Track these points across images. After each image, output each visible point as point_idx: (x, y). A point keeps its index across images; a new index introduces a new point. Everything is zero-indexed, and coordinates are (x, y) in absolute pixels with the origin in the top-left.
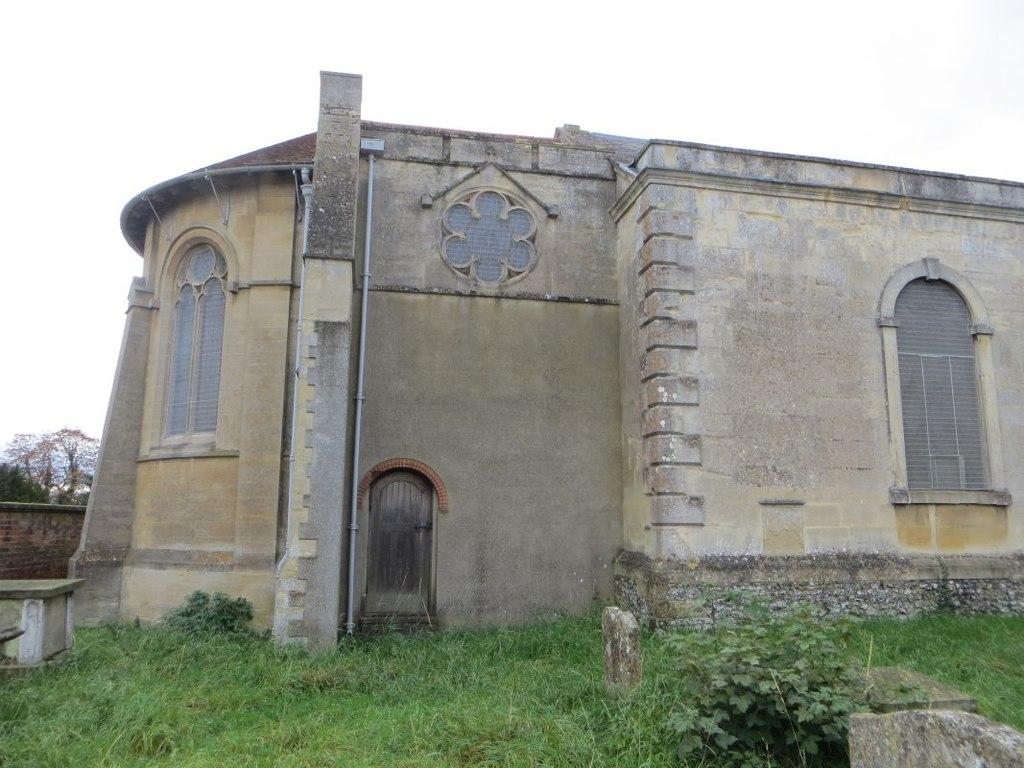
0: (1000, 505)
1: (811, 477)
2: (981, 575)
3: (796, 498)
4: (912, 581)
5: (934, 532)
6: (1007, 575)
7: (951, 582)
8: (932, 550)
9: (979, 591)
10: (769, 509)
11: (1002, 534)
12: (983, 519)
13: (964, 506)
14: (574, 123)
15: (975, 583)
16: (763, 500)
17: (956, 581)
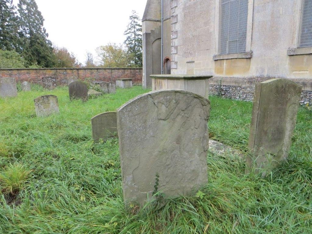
0: (249, 58)
1: (196, 54)
2: (232, 85)
3: (193, 60)
4: (212, 85)
5: (225, 69)
6: (240, 85)
7: (222, 86)
8: (223, 75)
9: (231, 90)
10: (189, 64)
11: (247, 69)
12: (241, 64)
13: (235, 59)
14: (41, 12)
15: (229, 87)
16: (193, 63)
17: (224, 86)
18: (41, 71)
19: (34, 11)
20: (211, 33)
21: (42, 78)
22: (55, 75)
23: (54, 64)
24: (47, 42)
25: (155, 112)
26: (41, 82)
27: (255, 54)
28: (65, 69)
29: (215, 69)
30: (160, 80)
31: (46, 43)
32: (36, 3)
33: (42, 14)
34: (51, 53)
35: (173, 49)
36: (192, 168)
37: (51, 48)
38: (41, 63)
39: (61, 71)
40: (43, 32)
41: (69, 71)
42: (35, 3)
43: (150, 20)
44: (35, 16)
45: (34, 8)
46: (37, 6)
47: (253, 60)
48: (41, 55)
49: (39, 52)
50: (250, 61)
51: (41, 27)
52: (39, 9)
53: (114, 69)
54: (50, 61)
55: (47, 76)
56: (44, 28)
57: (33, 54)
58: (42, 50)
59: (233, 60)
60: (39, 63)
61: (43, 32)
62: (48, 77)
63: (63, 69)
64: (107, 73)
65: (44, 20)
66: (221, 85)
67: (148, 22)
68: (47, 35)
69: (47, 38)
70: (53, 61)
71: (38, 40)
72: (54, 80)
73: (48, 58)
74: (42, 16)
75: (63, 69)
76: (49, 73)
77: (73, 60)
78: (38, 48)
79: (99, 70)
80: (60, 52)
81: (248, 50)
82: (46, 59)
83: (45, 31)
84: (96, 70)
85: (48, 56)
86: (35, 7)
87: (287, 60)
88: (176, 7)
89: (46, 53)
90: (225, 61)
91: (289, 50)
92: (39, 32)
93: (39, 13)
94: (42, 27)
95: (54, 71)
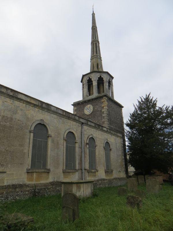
0: (48, 172)
3: (5, 171)
5: (34, 178)
11: (48, 178)
12: (44, 175)
15: (41, 189)
17: (37, 189)
20: (25, 153)
27: (51, 170)
29: (27, 179)
30: (80, 184)
33: (102, 59)
47: (50, 174)
59: (40, 173)
66: (35, 189)
87: (62, 174)
90: (35, 173)
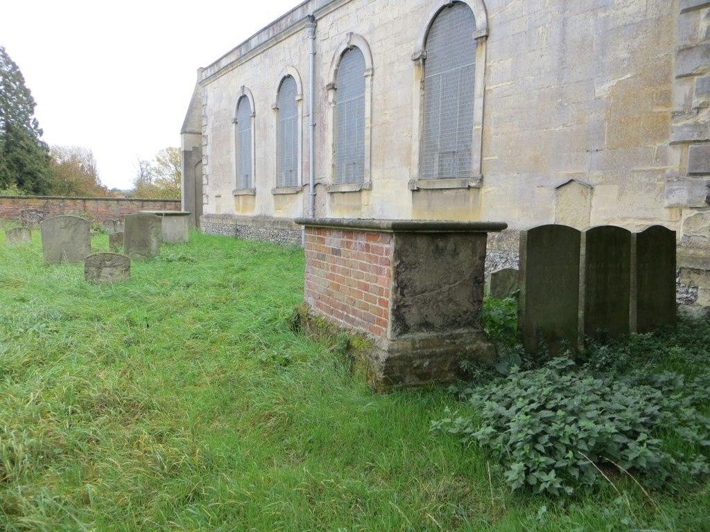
18: (21, 201)
19: (17, 88)
21: (22, 212)
22: (44, 207)
23: (50, 186)
24: (39, 145)
25: (700, 417)
26: (20, 217)
28: (63, 199)
31: (37, 147)
32: (22, 72)
33: (32, 94)
34: (45, 167)
35: (204, 178)
36: (82, 253)
37: (47, 157)
38: (25, 184)
39: (54, 201)
40: (33, 126)
41: (68, 202)
42: (19, 74)
43: (191, 133)
44: (18, 97)
45: (18, 83)
46: (23, 79)
48: (26, 170)
49: (22, 164)
50: (360, 196)
51: (30, 118)
52: (27, 85)
53: (147, 201)
54: (44, 182)
55: (31, 208)
56: (35, 119)
57: (10, 167)
58: (28, 160)
60: (20, 183)
61: (33, 126)
62: (32, 211)
63: (58, 198)
64: (136, 209)
65: (35, 104)
67: (187, 135)
68: (41, 132)
69: (41, 139)
70: (50, 181)
71: (21, 142)
72: (41, 215)
73: (40, 175)
74: (32, 98)
75: (58, 198)
76: (36, 203)
77: (91, 177)
78: (21, 157)
79: (120, 202)
80: (66, 165)
81: (253, 187)
82: (35, 178)
83: (36, 124)
84: (115, 202)
85: (39, 171)
86: (19, 81)
88: (206, 125)
89: (36, 166)
91: (412, 182)
92: (25, 126)
93: (27, 92)
94: (32, 117)
95: (43, 201)
